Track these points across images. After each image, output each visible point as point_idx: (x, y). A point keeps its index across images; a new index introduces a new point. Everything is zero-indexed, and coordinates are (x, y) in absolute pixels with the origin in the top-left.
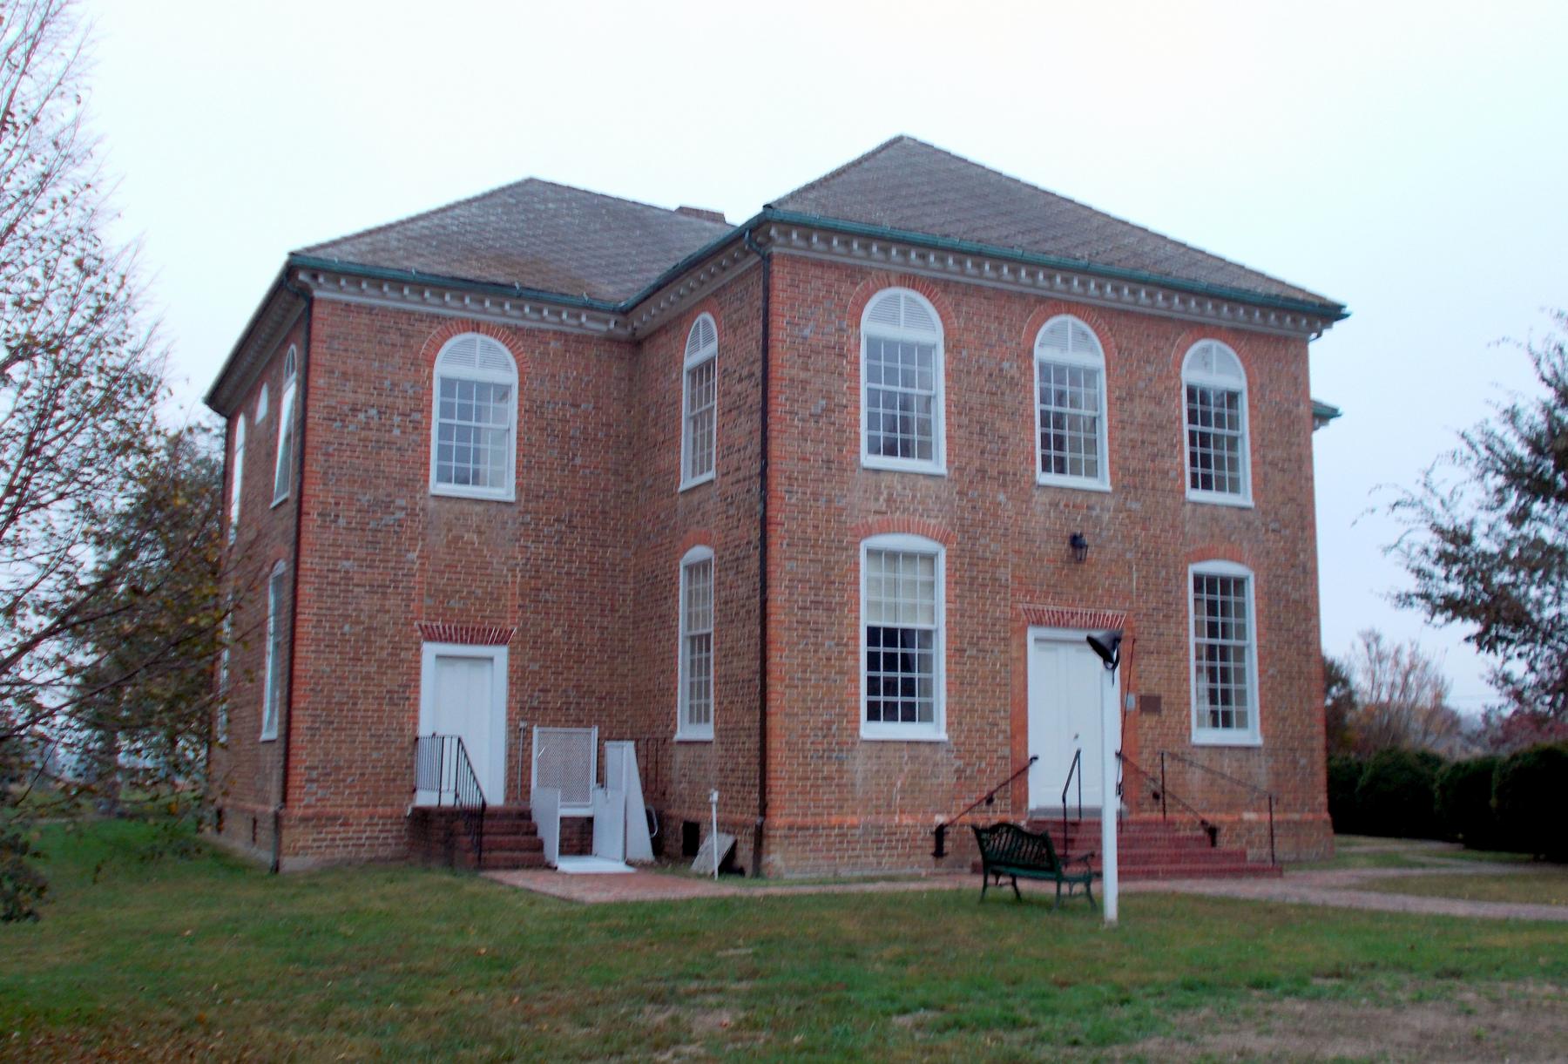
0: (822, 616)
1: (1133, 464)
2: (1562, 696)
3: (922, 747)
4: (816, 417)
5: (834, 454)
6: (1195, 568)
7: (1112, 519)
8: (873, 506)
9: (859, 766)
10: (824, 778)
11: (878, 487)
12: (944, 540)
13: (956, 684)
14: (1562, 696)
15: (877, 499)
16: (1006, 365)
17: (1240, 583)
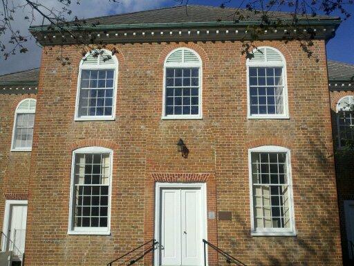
0: (52, 183)
1: (215, 106)
2: (3, 250)
3: (98, 237)
4: (55, 104)
5: (62, 117)
6: (250, 151)
7: (202, 132)
8: (80, 136)
9: (66, 247)
10: (50, 251)
11: (81, 128)
12: (112, 148)
13: (117, 209)
14: (3, 250)
15: (81, 133)
16: (148, 72)
17: (282, 157)
